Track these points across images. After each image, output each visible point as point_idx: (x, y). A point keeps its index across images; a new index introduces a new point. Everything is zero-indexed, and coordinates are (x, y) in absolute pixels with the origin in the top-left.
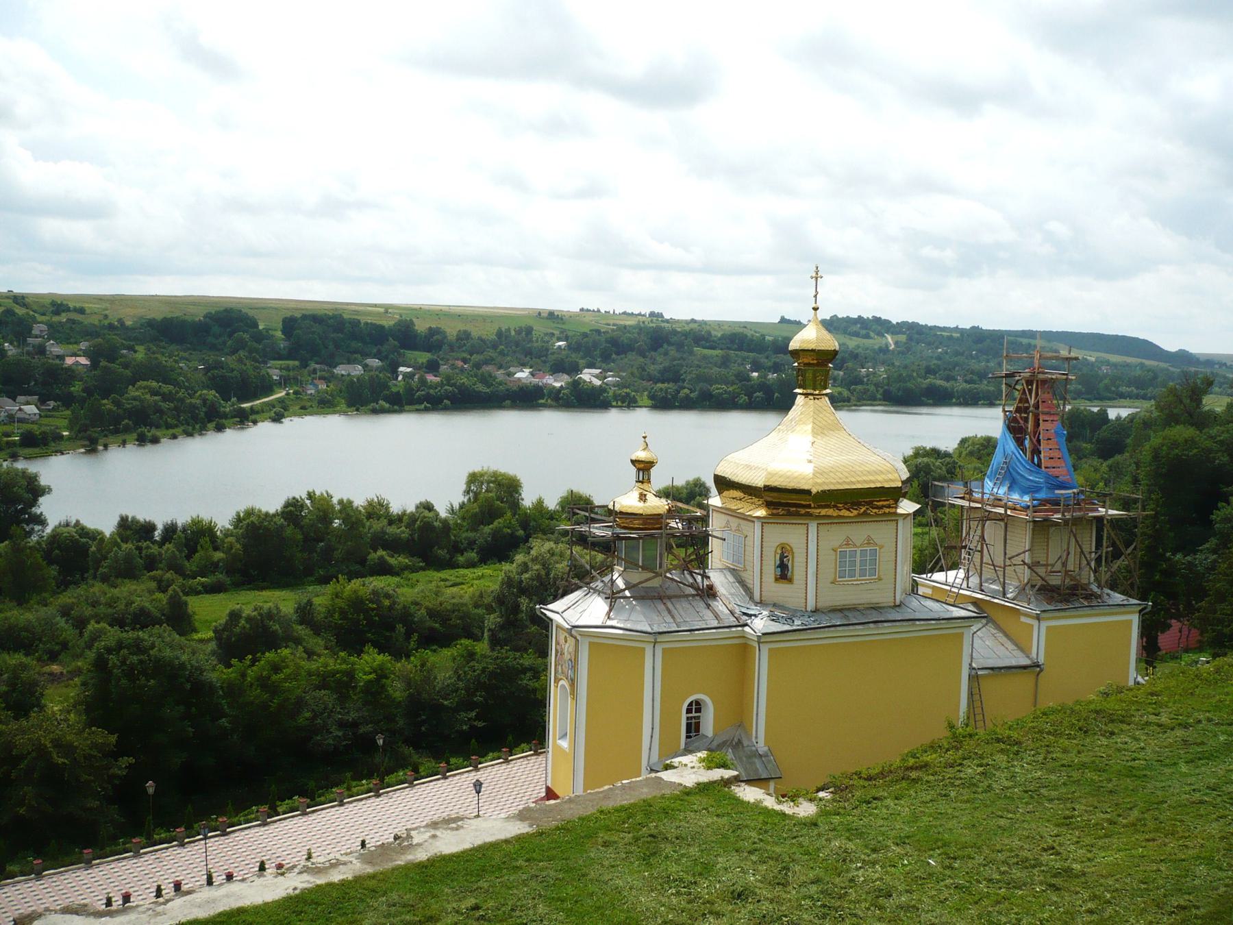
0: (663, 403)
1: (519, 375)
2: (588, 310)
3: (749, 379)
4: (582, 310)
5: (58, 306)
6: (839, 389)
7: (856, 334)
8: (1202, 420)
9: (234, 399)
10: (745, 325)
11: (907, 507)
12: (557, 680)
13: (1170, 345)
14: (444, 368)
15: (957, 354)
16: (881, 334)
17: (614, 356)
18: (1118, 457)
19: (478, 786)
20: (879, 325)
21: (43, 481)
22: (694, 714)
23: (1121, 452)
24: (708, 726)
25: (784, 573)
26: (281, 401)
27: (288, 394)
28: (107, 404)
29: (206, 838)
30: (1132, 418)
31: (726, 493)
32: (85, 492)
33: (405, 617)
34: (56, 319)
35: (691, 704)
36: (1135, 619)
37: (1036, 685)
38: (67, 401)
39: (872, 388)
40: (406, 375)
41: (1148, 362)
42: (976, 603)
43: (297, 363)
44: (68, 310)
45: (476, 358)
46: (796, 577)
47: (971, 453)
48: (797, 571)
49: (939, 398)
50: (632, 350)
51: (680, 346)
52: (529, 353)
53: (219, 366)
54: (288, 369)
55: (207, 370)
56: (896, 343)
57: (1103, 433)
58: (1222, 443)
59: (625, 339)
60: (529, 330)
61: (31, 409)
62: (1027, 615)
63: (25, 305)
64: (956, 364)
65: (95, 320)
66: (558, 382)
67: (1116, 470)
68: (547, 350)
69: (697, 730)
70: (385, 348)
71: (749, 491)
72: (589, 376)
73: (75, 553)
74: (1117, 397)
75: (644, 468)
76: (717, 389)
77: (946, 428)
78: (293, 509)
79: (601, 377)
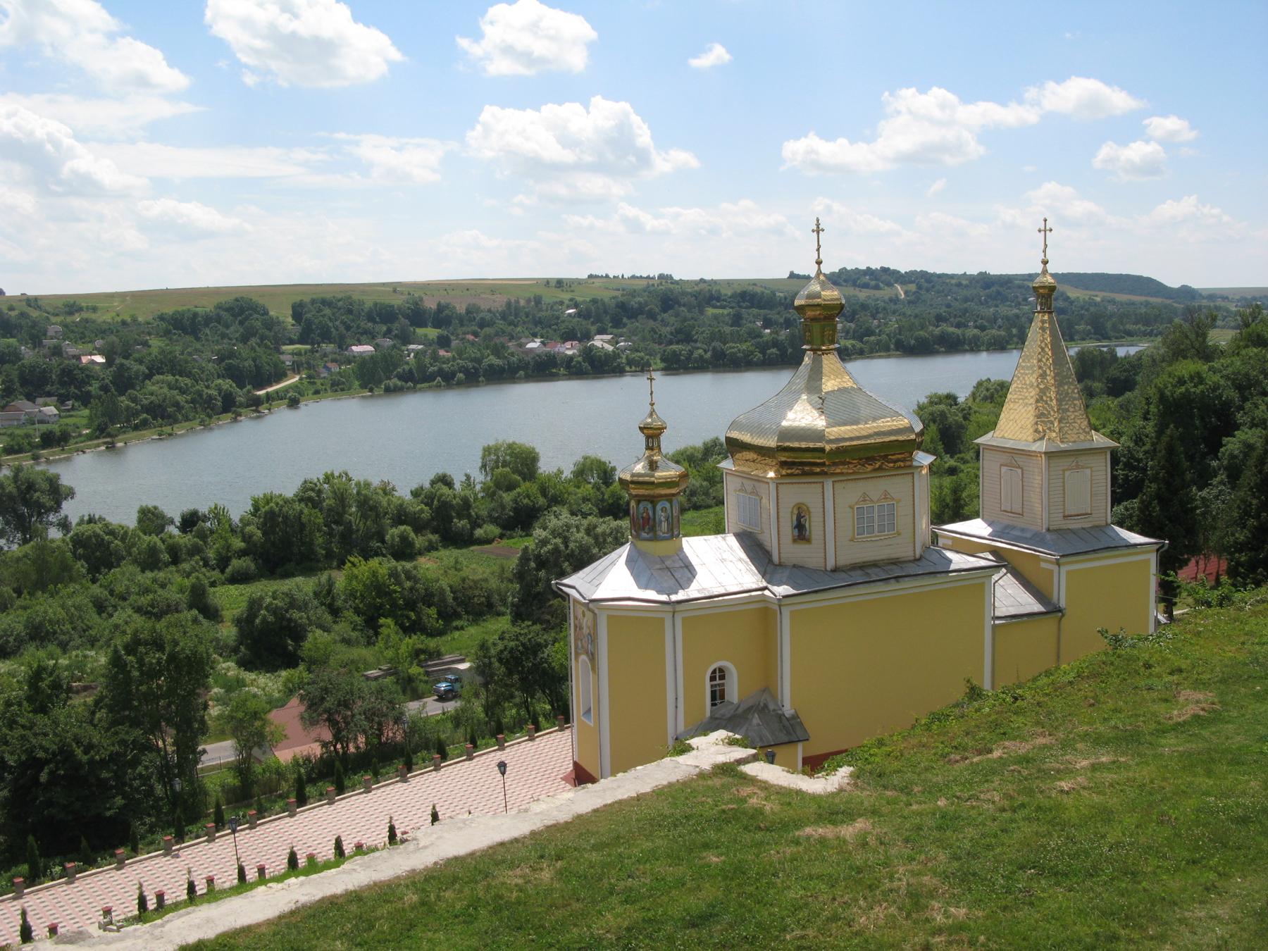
0: (675, 365)
1: (530, 345)
2: (597, 277)
3: (760, 335)
4: (591, 276)
5: (71, 305)
6: (851, 341)
7: (866, 286)
8: (1207, 354)
9: (249, 387)
10: (754, 283)
11: (924, 459)
12: (577, 655)
13: (1172, 280)
14: (455, 343)
15: (966, 300)
16: (889, 285)
17: (625, 320)
18: (1128, 394)
19: (502, 766)
20: (885, 276)
21: (66, 480)
22: (718, 682)
23: (1131, 389)
24: (734, 692)
25: (801, 532)
26: (294, 387)
27: (301, 379)
28: (124, 401)
29: (234, 832)
30: (1139, 356)
31: (738, 456)
32: (109, 486)
33: (428, 598)
34: (69, 319)
35: (714, 672)
36: (1153, 559)
37: (1059, 629)
38: (85, 400)
39: (884, 337)
40: (417, 353)
41: (1152, 300)
42: (995, 552)
43: (308, 347)
44: (80, 309)
45: (487, 330)
46: (813, 537)
47: (985, 399)
48: (815, 530)
49: (952, 346)
50: (642, 313)
51: (690, 308)
52: (538, 322)
53: (232, 355)
54: (299, 354)
55: (220, 360)
56: (906, 293)
57: (1113, 372)
58: (1227, 378)
59: (634, 303)
60: (538, 300)
61: (51, 410)
62: (1046, 561)
63: (39, 308)
64: (966, 311)
65: (107, 317)
66: (569, 349)
67: (1125, 407)
68: (558, 318)
69: (722, 697)
70: (396, 326)
71: (762, 451)
72: (601, 342)
73: (98, 550)
74: (1127, 335)
75: (652, 435)
76: (734, 348)
77: (957, 375)
78: (310, 495)
79: (614, 342)
